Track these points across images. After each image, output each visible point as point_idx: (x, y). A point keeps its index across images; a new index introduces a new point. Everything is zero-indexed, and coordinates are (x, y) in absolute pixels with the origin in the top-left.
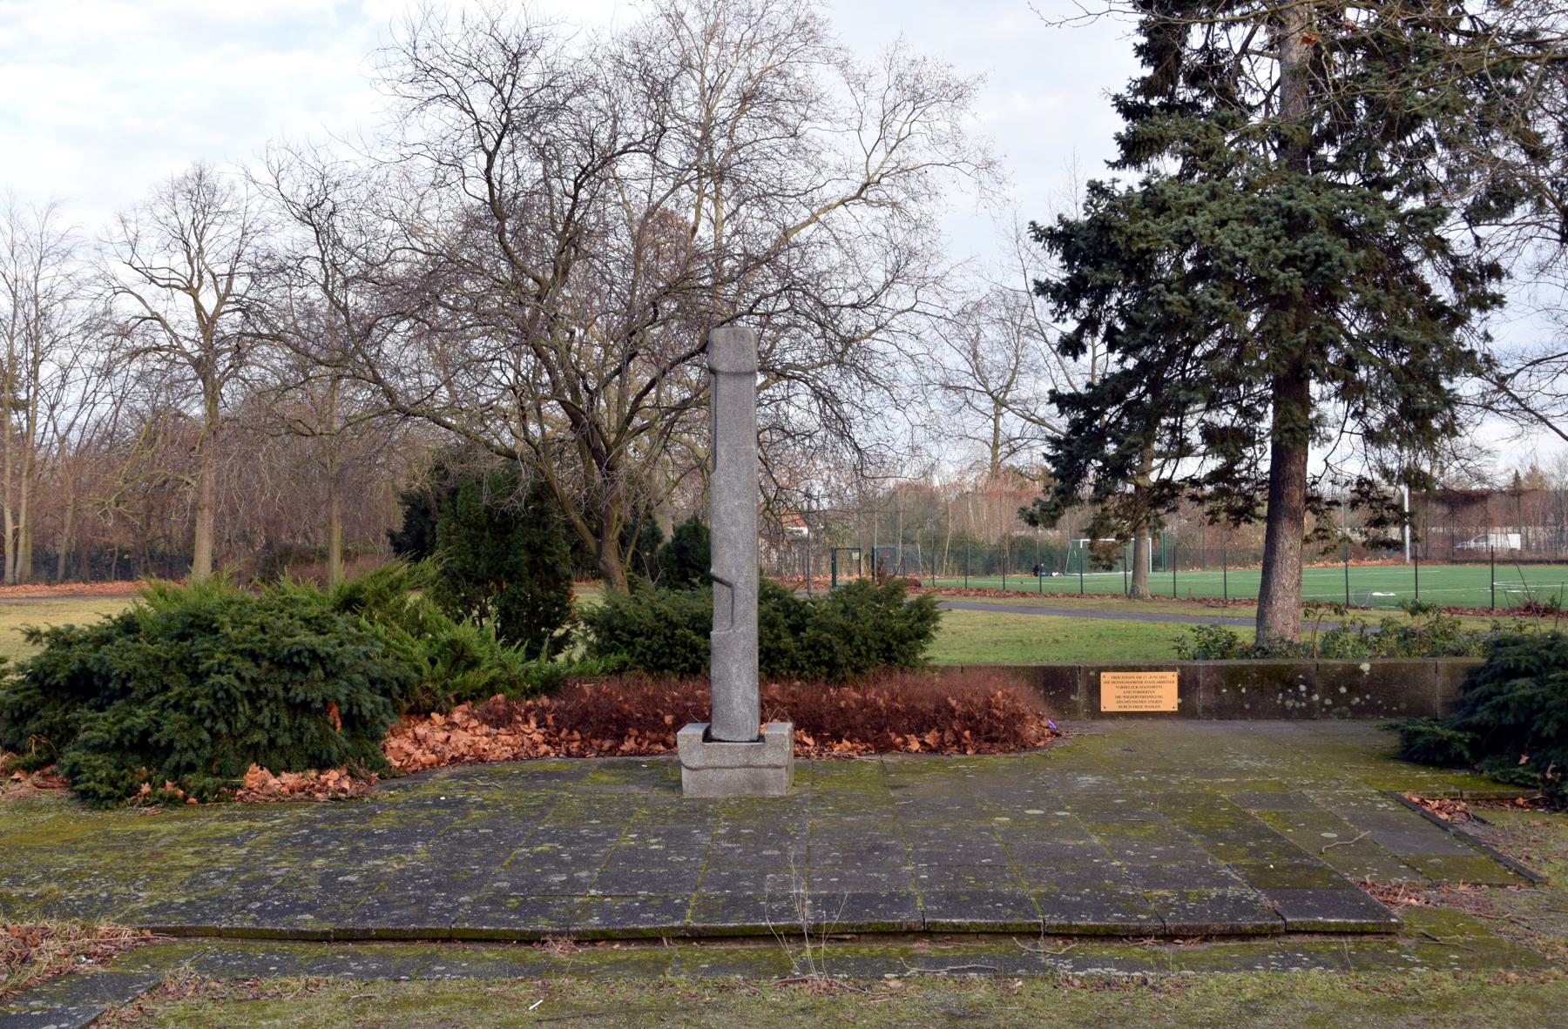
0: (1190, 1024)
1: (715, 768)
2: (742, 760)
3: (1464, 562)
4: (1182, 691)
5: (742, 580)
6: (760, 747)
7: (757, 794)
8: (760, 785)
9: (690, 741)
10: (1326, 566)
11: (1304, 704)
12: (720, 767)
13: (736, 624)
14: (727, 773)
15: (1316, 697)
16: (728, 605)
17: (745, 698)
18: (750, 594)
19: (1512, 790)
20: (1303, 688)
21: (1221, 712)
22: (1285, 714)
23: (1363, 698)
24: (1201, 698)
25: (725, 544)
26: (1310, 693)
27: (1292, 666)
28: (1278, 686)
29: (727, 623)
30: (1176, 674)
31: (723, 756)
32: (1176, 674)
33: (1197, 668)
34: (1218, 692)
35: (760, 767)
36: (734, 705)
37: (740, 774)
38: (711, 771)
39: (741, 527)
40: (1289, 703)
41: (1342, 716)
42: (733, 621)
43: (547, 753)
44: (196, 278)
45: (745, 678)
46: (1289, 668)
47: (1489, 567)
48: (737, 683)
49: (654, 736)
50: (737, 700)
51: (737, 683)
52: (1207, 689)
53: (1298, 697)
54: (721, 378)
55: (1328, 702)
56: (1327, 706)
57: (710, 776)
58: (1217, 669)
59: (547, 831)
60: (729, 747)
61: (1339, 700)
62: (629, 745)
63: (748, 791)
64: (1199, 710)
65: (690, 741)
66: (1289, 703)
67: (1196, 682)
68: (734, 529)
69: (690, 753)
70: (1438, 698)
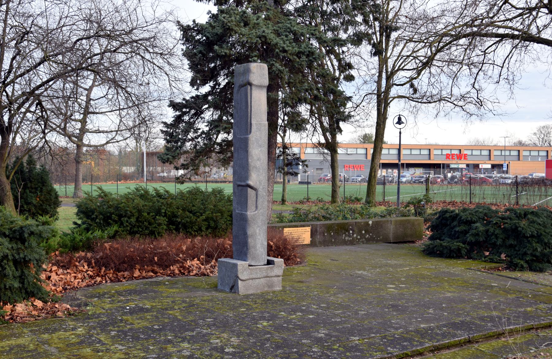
1: (252, 279)
2: (265, 274)
3: (169, 182)
4: (312, 236)
5: (261, 187)
7: (270, 290)
8: (271, 286)
9: (243, 266)
10: (112, 183)
12: (255, 279)
13: (259, 208)
15: (355, 235)
17: (262, 244)
18: (264, 194)
19: (497, 265)
20: (351, 232)
21: (326, 243)
22: (345, 243)
23: (369, 235)
24: (318, 238)
26: (353, 234)
27: (348, 223)
28: (343, 231)
29: (254, 208)
30: (310, 228)
31: (257, 273)
32: (310, 228)
33: (317, 225)
34: (324, 235)
35: (272, 277)
36: (257, 247)
38: (251, 281)
39: (262, 161)
40: (347, 238)
41: (363, 242)
42: (257, 207)
43: (101, 282)
44: (508, 31)
45: (262, 235)
46: (347, 223)
48: (259, 237)
49: (149, 268)
50: (259, 246)
52: (320, 234)
53: (349, 236)
54: (253, 88)
55: (359, 237)
56: (358, 239)
57: (250, 284)
58: (324, 225)
59: (268, 312)
60: (260, 268)
61: (361, 235)
62: (137, 273)
63: (266, 289)
64: (317, 243)
65: (243, 266)
66: (347, 238)
67: (316, 231)
68: (259, 162)
69: (243, 273)
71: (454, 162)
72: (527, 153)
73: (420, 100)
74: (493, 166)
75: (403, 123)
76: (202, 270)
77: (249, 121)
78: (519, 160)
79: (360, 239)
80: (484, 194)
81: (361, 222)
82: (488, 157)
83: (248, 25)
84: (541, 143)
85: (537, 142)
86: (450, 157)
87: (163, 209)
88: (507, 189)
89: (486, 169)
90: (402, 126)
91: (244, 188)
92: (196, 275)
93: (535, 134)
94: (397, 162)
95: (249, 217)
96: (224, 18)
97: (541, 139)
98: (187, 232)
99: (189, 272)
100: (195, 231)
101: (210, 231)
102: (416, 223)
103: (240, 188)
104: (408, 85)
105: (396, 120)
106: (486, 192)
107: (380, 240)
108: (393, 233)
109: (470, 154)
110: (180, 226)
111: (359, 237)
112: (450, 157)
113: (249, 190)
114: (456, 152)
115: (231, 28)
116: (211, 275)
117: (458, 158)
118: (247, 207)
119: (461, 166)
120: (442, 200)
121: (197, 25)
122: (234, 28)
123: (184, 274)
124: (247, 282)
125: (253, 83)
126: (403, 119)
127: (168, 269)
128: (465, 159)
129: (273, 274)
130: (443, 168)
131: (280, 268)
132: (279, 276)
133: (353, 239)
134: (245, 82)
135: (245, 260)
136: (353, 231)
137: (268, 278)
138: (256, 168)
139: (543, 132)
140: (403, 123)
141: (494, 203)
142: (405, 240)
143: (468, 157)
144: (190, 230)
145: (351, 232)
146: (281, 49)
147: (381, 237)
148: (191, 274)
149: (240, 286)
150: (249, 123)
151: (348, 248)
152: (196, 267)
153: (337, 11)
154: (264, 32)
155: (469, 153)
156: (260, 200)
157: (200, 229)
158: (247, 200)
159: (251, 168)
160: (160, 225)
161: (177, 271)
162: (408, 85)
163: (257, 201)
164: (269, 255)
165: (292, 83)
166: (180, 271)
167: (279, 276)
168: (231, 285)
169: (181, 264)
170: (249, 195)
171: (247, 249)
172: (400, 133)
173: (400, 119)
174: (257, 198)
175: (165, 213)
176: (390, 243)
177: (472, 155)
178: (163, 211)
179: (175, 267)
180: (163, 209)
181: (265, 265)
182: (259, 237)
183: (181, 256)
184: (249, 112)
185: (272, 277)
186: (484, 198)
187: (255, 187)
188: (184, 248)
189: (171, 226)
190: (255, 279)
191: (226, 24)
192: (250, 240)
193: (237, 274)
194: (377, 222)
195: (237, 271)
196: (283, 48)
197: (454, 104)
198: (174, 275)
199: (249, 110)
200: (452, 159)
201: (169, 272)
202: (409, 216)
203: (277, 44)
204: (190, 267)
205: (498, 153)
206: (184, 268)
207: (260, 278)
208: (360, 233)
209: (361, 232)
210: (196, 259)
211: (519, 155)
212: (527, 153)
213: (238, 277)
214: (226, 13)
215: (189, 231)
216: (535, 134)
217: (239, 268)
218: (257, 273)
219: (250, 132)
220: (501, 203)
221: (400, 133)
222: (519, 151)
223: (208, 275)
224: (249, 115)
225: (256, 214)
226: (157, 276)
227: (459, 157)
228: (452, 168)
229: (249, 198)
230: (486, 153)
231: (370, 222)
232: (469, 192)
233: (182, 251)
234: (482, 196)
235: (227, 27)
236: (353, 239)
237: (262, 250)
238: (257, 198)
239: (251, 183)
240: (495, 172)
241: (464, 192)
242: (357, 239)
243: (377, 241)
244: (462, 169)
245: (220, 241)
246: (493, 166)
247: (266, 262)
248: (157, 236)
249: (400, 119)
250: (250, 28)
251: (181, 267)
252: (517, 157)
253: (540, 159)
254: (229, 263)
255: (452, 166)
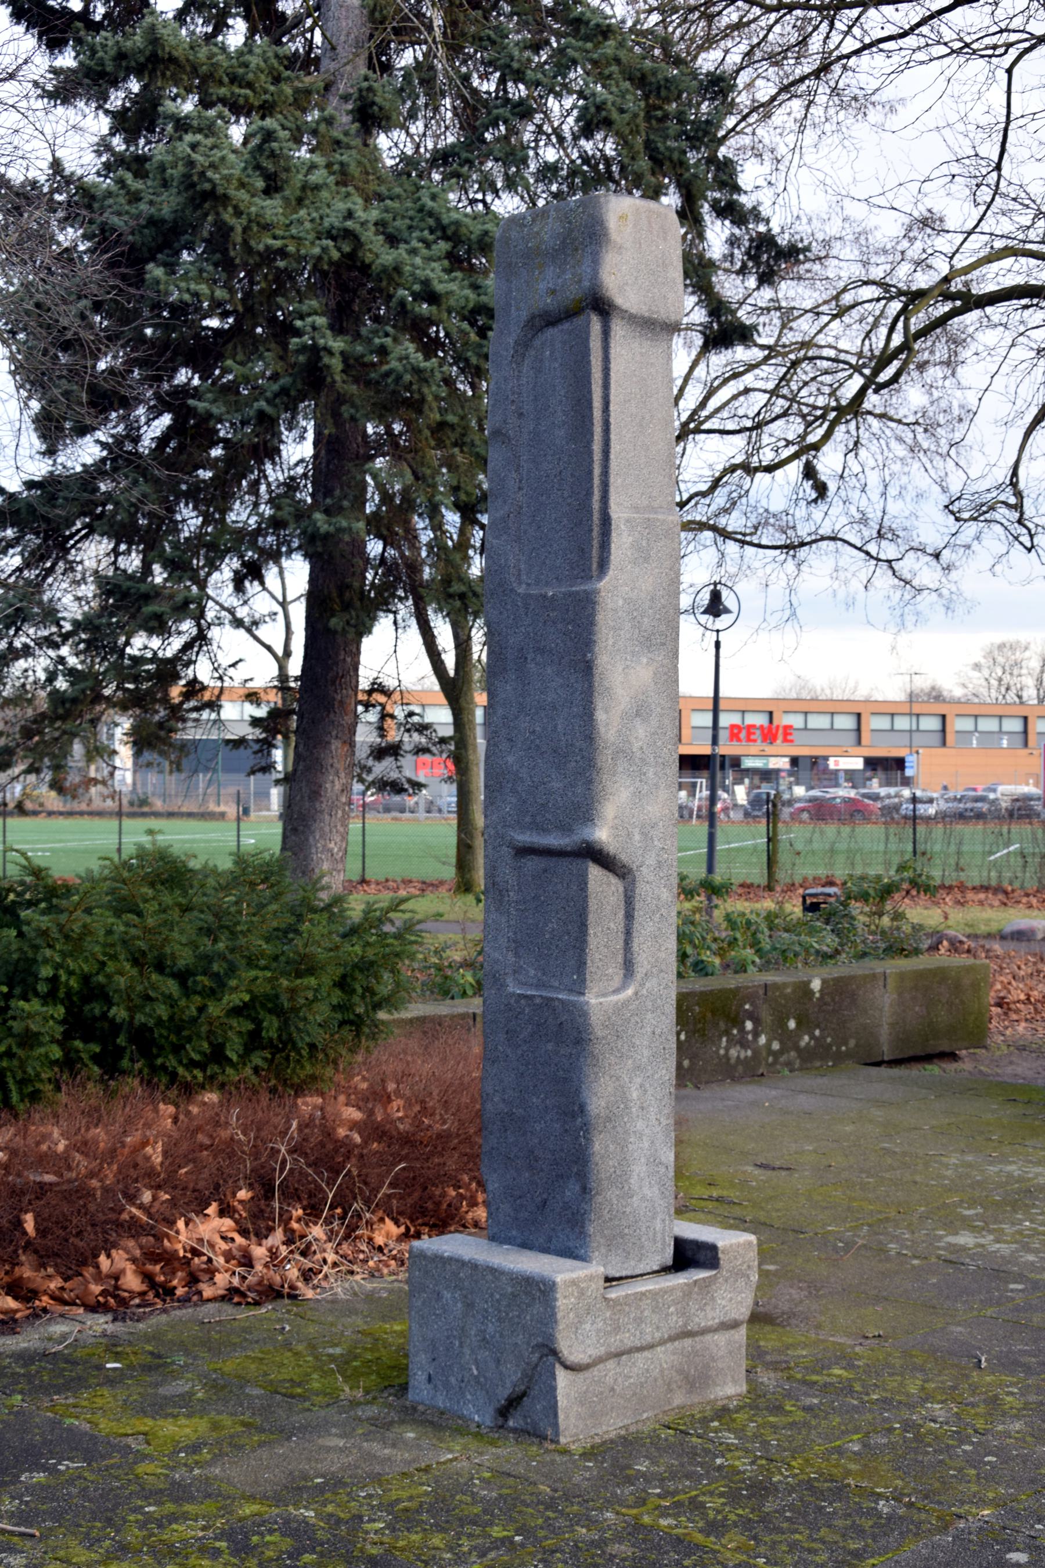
0: (348, 1559)
1: (618, 1355)
2: (675, 1322)
5: (651, 860)
6: (706, 1283)
9: (582, 1293)
11: (749, 1053)
12: (630, 1351)
13: (640, 971)
14: (641, 1360)
15: (763, 1040)
16: (617, 924)
17: (654, 1161)
20: (749, 1025)
23: (812, 1037)
25: (622, 766)
26: (756, 1034)
28: (722, 1025)
29: (615, 971)
35: (704, 1331)
37: (665, 1357)
38: (611, 1364)
40: (733, 1053)
42: (629, 966)
47: (114, 823)
50: (639, 1169)
51: (640, 1125)
53: (744, 1044)
54: (619, 329)
60: (654, 1294)
61: (789, 1040)
63: (679, 1399)
66: (733, 1053)
70: (886, 1027)
71: (754, 749)
72: (967, 725)
73: (748, 538)
74: (872, 763)
75: (727, 611)
76: (259, 1267)
77: (596, 505)
78: (944, 743)
79: (781, 1052)
80: (959, 853)
81: (785, 985)
82: (853, 736)
83: (278, 189)
84: (994, 694)
85: (984, 691)
86: (743, 735)
87: (46, 961)
88: (1034, 834)
89: (850, 775)
90: (724, 620)
91: (563, 865)
92: (232, 1295)
93: (977, 667)
94: (706, 750)
95: (596, 1018)
96: (194, 146)
97: (994, 683)
98: (154, 1069)
99: (193, 1280)
100: (192, 1064)
101: (257, 1059)
102: (966, 981)
103: (533, 864)
104: (795, 469)
105: (705, 597)
106: (965, 848)
107: (848, 1055)
108: (892, 1025)
109: (801, 725)
110: (121, 1041)
111: (776, 1046)
112: (743, 735)
113: (595, 872)
114: (760, 720)
115: (220, 190)
116: (310, 1294)
117: (764, 740)
118: (581, 965)
119: (774, 763)
120: (822, 872)
121: (68, 180)
122: (232, 192)
123: (171, 1291)
124: (595, 1371)
125: (619, 301)
126: (728, 599)
127: (89, 1272)
128: (785, 740)
129: (711, 1317)
130: (722, 767)
131: (741, 1283)
132: (735, 1325)
133: (756, 1053)
134: (572, 292)
135: (569, 1253)
136: (756, 1021)
137: (688, 1342)
138: (630, 757)
139: (1001, 660)
140: (727, 611)
141: (994, 883)
142: (929, 1050)
143: (795, 736)
144: (172, 1062)
145: (749, 1025)
146: (417, 287)
147: (852, 1043)
148: (208, 1292)
149: (562, 1402)
150: (596, 517)
151: (745, 1093)
152: (228, 1256)
153: (595, 168)
154: (350, 215)
155: (796, 721)
156: (645, 927)
157: (218, 1055)
158: (583, 927)
159: (605, 759)
160: (29, 1040)
161: (132, 1281)
162: (795, 469)
163: (628, 933)
164: (681, 1211)
165: (452, 427)
166: (148, 1278)
167: (735, 1325)
168: (503, 1394)
169: (148, 1240)
170: (593, 904)
171: (585, 1189)
172: (718, 644)
173: (716, 596)
174: (629, 916)
175: (54, 980)
176: (878, 1064)
177: (832, 729)
178: (46, 972)
179: (118, 1255)
180: (46, 961)
181: (665, 1270)
182: (640, 1125)
183: (147, 1197)
184: (597, 456)
185: (704, 1331)
186: (959, 868)
187: (623, 857)
188: (155, 1154)
189: (78, 1044)
190: (630, 1351)
191: (202, 174)
192: (600, 1145)
193: (551, 1338)
194: (838, 980)
195: (550, 1317)
196: (426, 283)
197: (867, 553)
198: (123, 1302)
199: (597, 447)
200: (749, 740)
201: (96, 1289)
202: (917, 952)
203: (397, 269)
204: (196, 1252)
205: (883, 723)
206: (169, 1259)
207: (651, 1347)
208: (779, 1029)
209: (783, 1024)
210: (212, 1210)
211: (944, 731)
212: (967, 725)
213: (554, 1353)
214: (200, 130)
215: (164, 1067)
216: (977, 667)
217: (563, 1302)
218: (639, 1321)
219: (603, 565)
220: (1017, 884)
221: (718, 644)
222: (944, 717)
223: (293, 1297)
224: (597, 471)
225: (626, 1003)
226: (36, 1315)
227: (769, 734)
228: (748, 770)
229: (591, 918)
230: (846, 722)
231: (816, 985)
232: (910, 848)
233: (151, 1173)
234: (952, 861)
235: (207, 186)
236: (756, 1053)
237: (651, 1191)
238: (629, 916)
239: (602, 834)
240: (875, 782)
241: (893, 847)
242: (770, 1052)
243: (839, 1058)
244: (777, 771)
245: (309, 1104)
246: (872, 763)
247: (667, 1256)
248: (15, 1097)
249: (716, 596)
250: (286, 199)
251: (152, 1256)
252: (939, 736)
253: (1005, 743)
254: (494, 1272)
255: (748, 763)
